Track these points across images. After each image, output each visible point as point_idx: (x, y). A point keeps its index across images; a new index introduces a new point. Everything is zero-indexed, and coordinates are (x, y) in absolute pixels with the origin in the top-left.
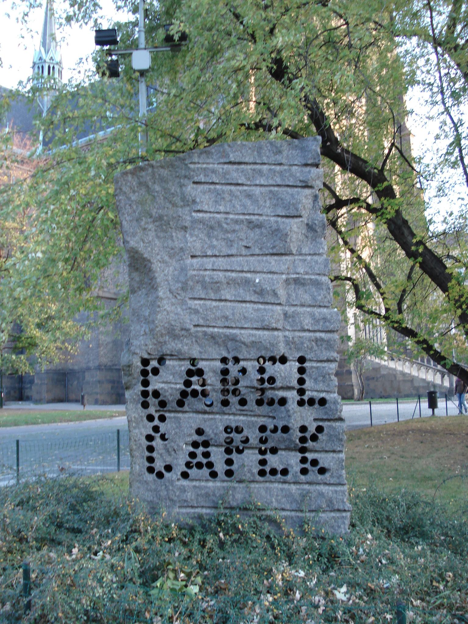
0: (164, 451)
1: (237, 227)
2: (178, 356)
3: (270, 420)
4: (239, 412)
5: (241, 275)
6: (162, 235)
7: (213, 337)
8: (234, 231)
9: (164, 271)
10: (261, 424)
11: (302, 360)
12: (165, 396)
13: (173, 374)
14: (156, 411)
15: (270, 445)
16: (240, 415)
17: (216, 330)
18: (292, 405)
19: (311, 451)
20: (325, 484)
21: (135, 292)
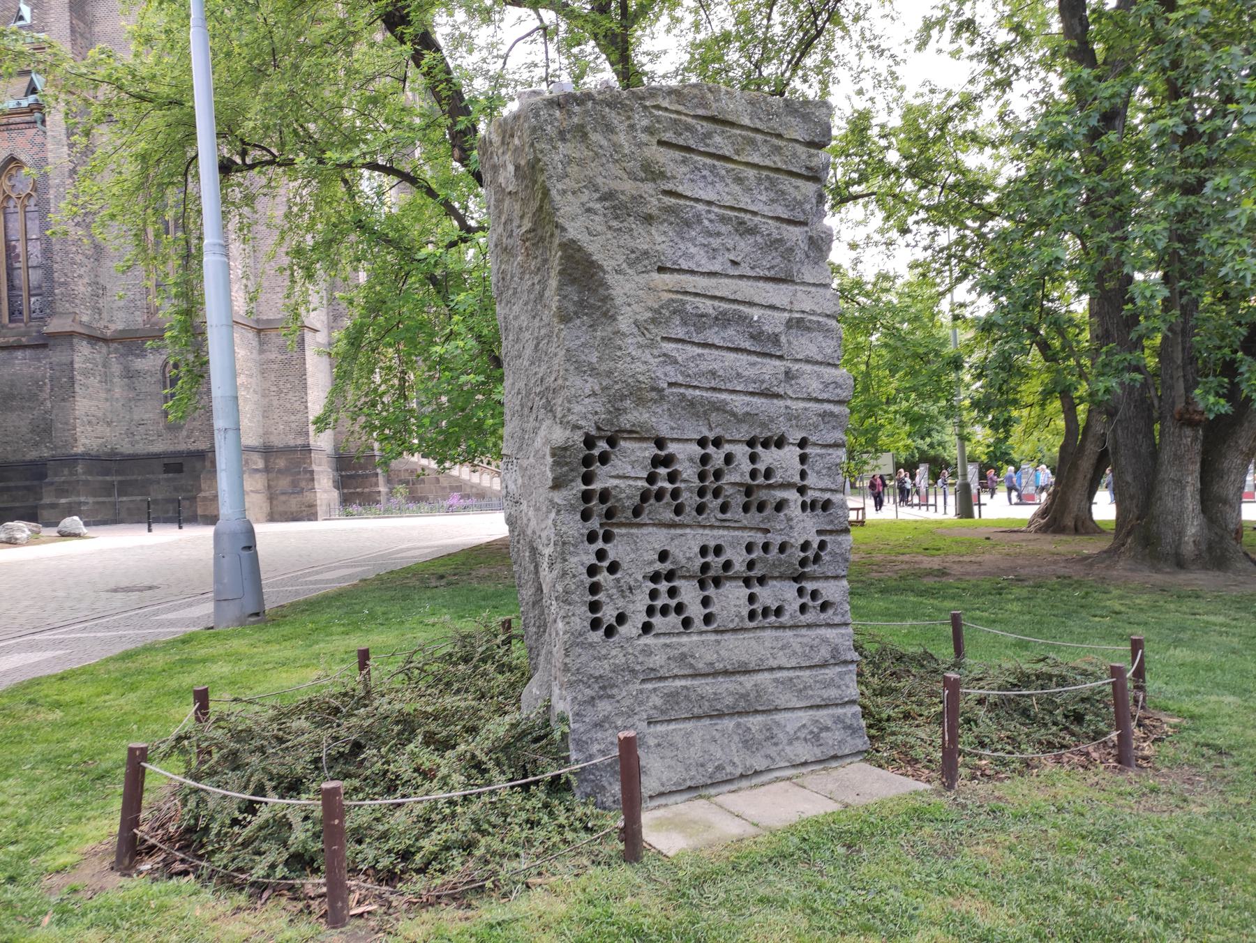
0: (614, 591)
1: (723, 229)
2: (635, 434)
3: (760, 535)
4: (717, 524)
5: (735, 307)
6: (615, 224)
7: (692, 404)
8: (719, 234)
9: (630, 291)
10: (749, 540)
11: (803, 443)
12: (618, 500)
13: (633, 464)
14: (602, 525)
15: (757, 572)
16: (719, 527)
17: (697, 392)
18: (794, 510)
19: (815, 579)
20: (829, 625)
21: (570, 320)
